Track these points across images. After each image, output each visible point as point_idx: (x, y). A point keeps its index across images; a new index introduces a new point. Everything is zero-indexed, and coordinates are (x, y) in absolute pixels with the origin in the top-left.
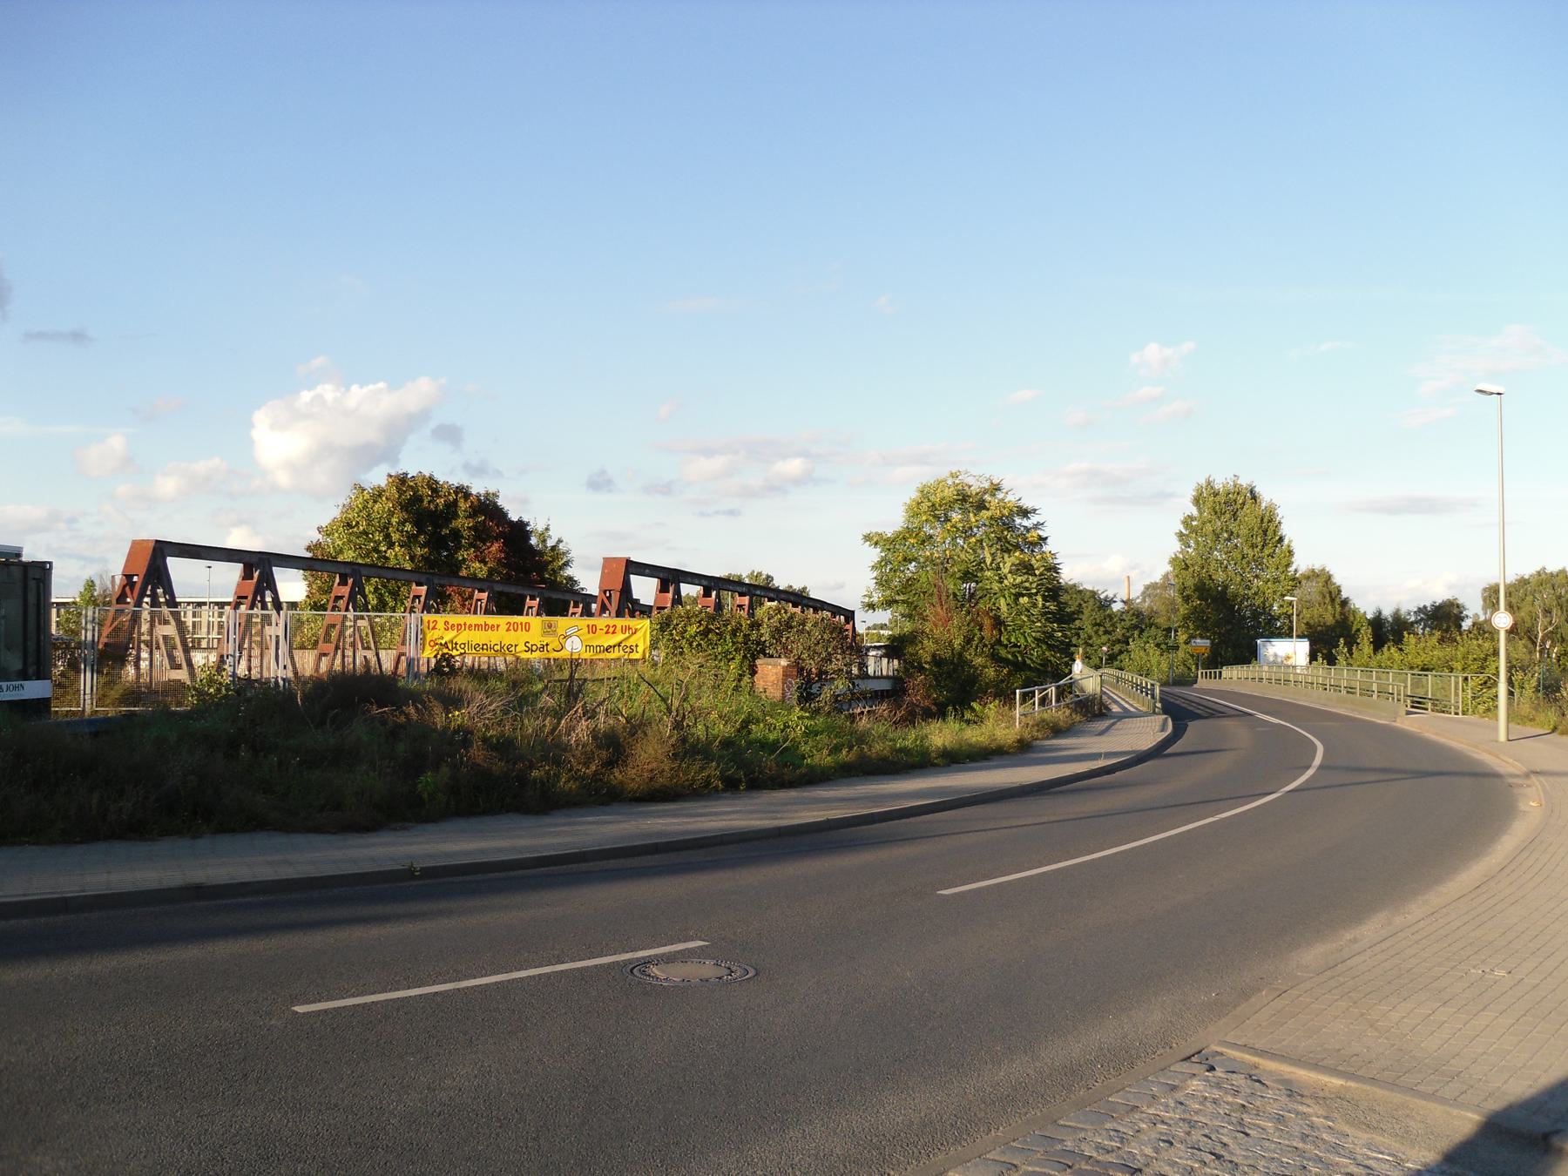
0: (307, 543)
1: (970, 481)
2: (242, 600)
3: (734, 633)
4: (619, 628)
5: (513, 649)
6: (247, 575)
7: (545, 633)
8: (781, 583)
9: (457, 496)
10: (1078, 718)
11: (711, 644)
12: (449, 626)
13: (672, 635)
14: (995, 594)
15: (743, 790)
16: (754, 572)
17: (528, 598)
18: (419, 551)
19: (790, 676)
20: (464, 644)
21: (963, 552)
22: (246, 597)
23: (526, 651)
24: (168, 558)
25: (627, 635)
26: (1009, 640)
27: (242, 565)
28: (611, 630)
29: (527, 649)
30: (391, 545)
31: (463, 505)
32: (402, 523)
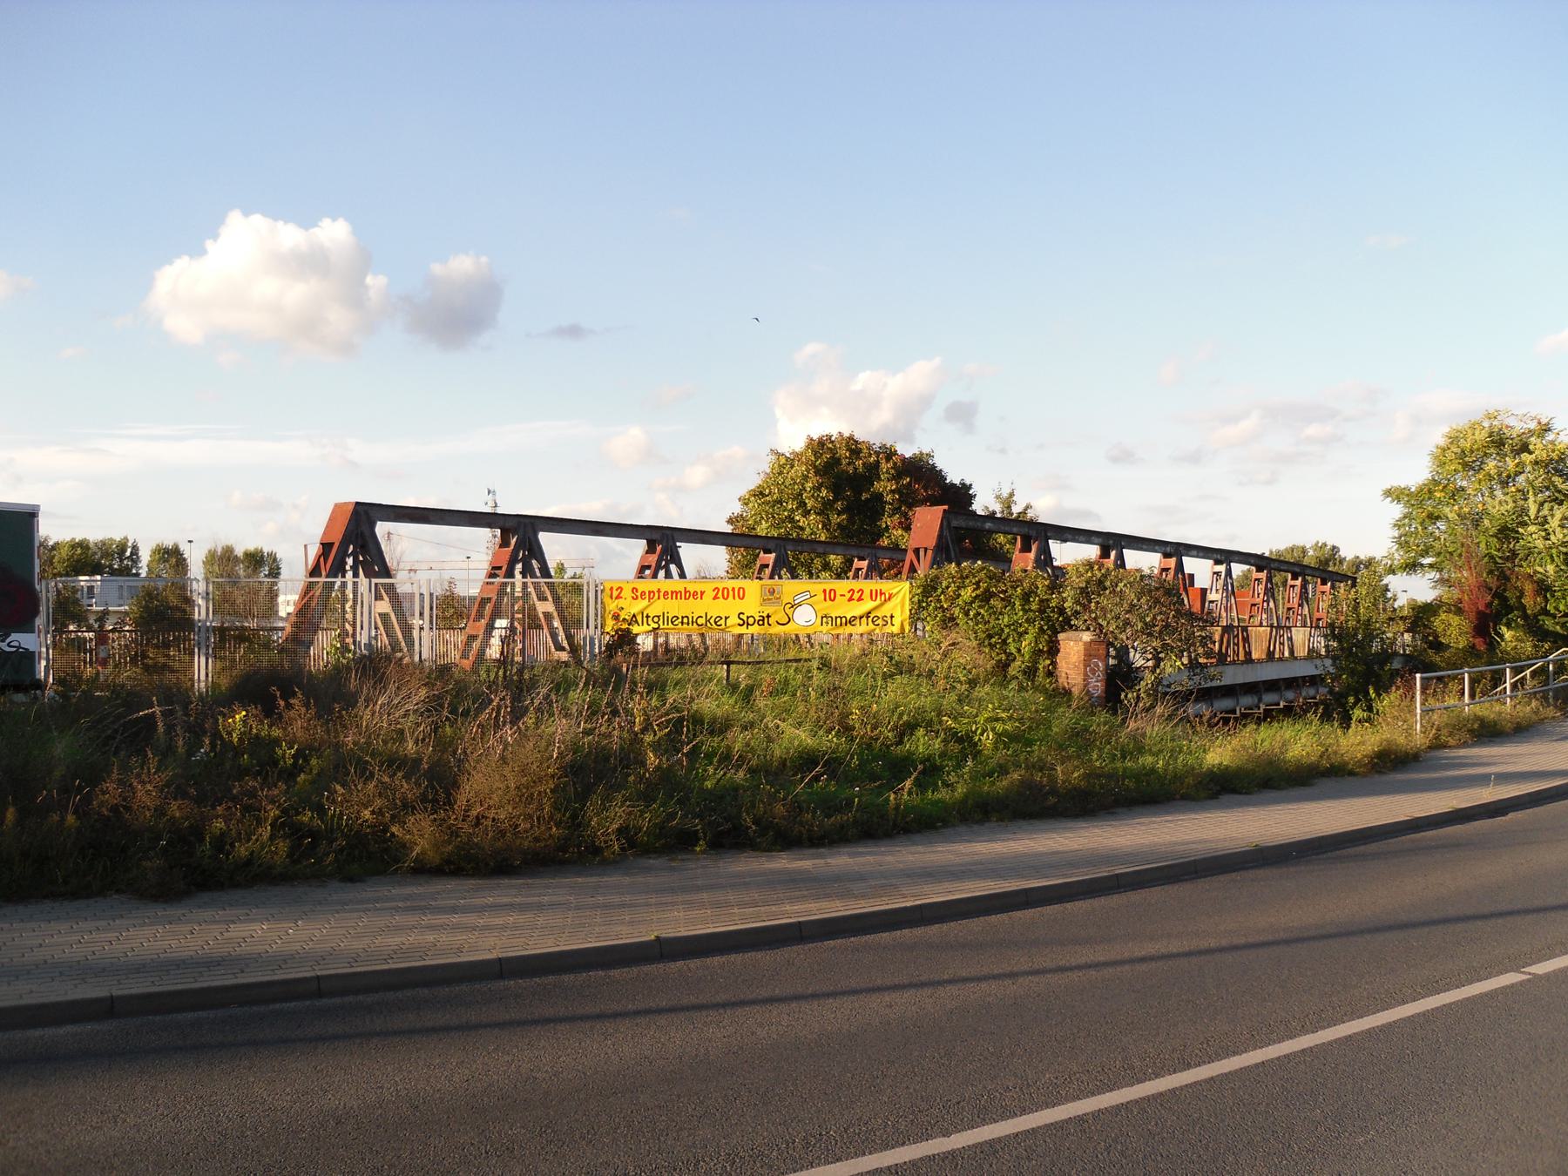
0: (727, 515)
1: (1511, 422)
2: (496, 572)
3: (1026, 597)
4: (867, 593)
5: (722, 622)
6: (651, 549)
7: (765, 601)
9: (878, 457)
10: (1551, 712)
11: (995, 613)
12: (639, 594)
13: (939, 601)
14: (1539, 553)
15: (703, 852)
16: (1318, 542)
18: (835, 519)
19: (1095, 656)
20: (658, 617)
21: (1500, 505)
22: (500, 568)
23: (739, 625)
24: (379, 523)
25: (878, 602)
26: (1556, 608)
28: (855, 597)
29: (741, 622)
30: (806, 513)
31: (884, 466)
32: (818, 488)
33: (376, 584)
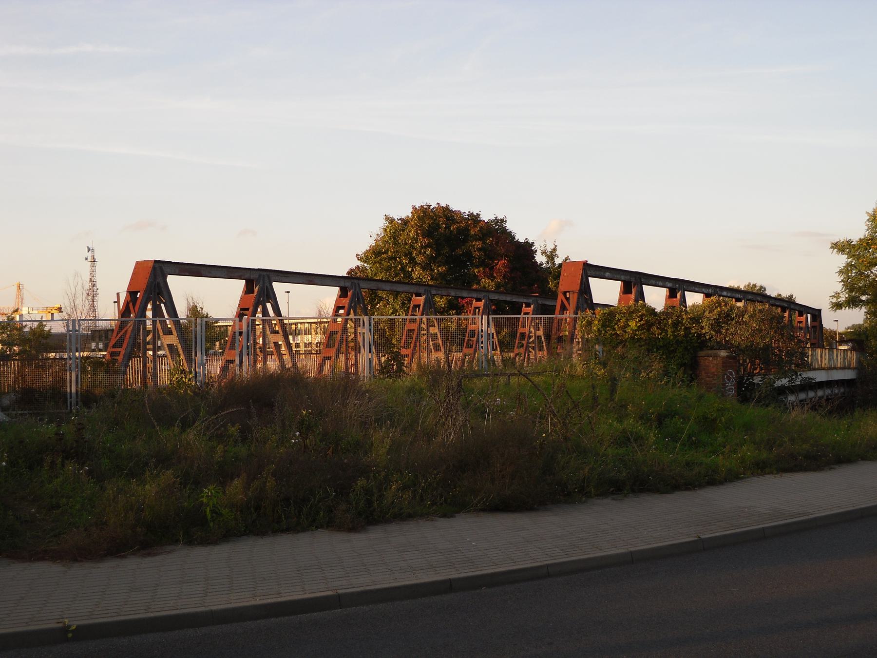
6: (249, 289)
8: (772, 292)
17: (524, 305)
22: (247, 309)
24: (169, 276)
27: (244, 281)
33: (492, 318)
